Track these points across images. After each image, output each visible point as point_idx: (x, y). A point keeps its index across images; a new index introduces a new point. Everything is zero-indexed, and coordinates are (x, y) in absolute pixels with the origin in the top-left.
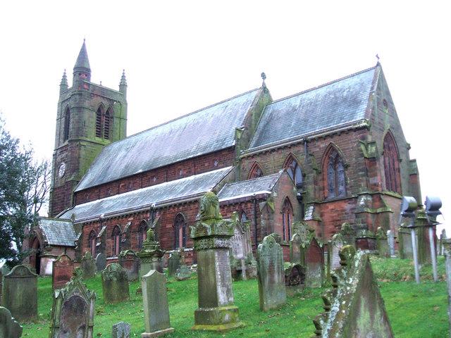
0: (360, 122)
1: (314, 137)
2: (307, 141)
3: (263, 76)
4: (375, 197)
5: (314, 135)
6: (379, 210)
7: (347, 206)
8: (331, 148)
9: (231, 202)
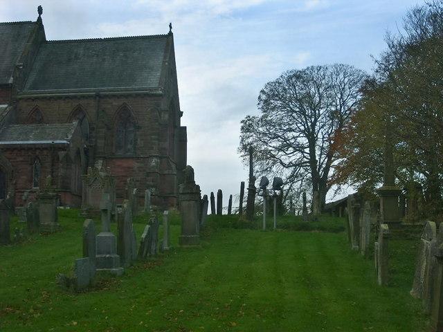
0: (156, 89)
1: (107, 93)
2: (100, 97)
3: (40, 10)
4: (164, 160)
5: (118, 91)
6: (166, 172)
7: (136, 165)
8: (124, 108)
9: (60, 146)
